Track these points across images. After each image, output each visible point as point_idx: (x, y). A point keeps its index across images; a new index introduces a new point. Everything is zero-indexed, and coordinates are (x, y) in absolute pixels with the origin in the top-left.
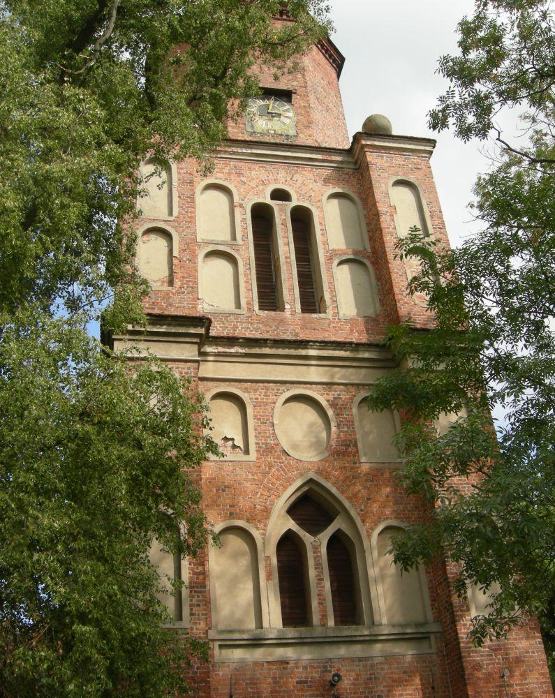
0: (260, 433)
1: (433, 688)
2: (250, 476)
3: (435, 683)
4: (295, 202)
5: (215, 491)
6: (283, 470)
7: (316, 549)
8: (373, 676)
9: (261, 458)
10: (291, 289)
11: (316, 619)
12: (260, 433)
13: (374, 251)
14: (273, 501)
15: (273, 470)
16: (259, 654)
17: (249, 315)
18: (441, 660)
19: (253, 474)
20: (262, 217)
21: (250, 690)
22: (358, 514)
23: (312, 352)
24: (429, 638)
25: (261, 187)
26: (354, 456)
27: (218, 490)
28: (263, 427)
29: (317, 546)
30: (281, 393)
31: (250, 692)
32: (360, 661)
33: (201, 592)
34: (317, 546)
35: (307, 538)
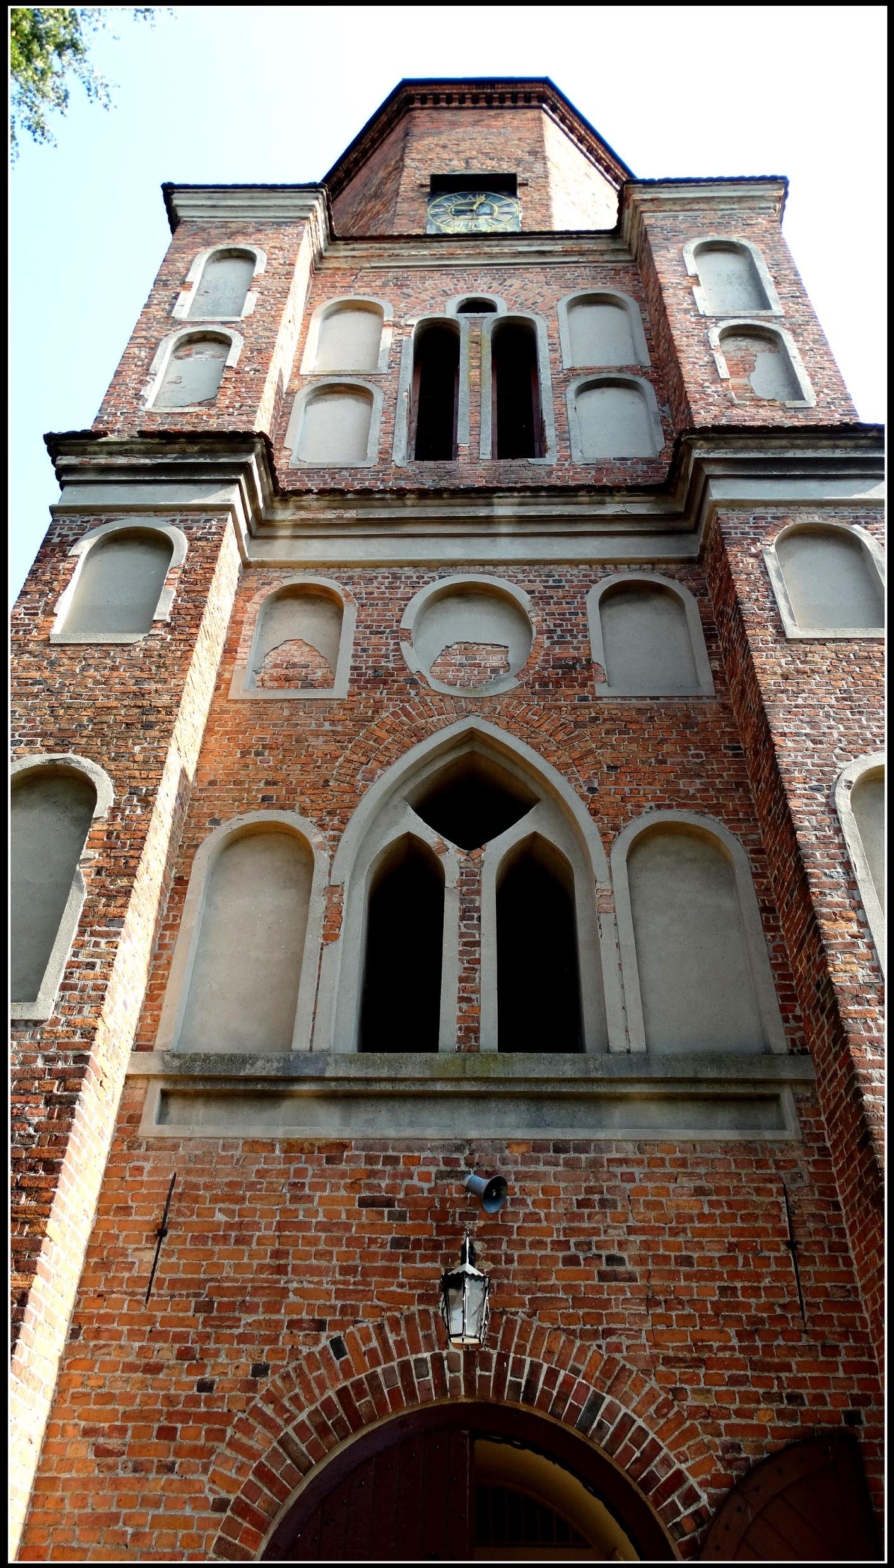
0: (364, 650)
1: (792, 1245)
2: (327, 726)
3: (800, 1231)
4: (503, 311)
5: (239, 755)
6: (407, 714)
7: (470, 880)
8: (596, 1197)
9: (360, 694)
10: (476, 427)
11: (449, 1032)
12: (364, 650)
13: (657, 365)
14: (372, 772)
15: (384, 715)
16: (556, 1134)
17: (382, 468)
18: (815, 1163)
19: (333, 723)
20: (436, 346)
21: (220, 1217)
22: (583, 797)
23: (504, 529)
24: (775, 1099)
25: (439, 299)
26: (583, 685)
27: (244, 754)
28: (374, 639)
29: (472, 878)
30: (427, 583)
31: (219, 1224)
32: (557, 1150)
33: (106, 935)
34: (472, 878)
35: (452, 860)
